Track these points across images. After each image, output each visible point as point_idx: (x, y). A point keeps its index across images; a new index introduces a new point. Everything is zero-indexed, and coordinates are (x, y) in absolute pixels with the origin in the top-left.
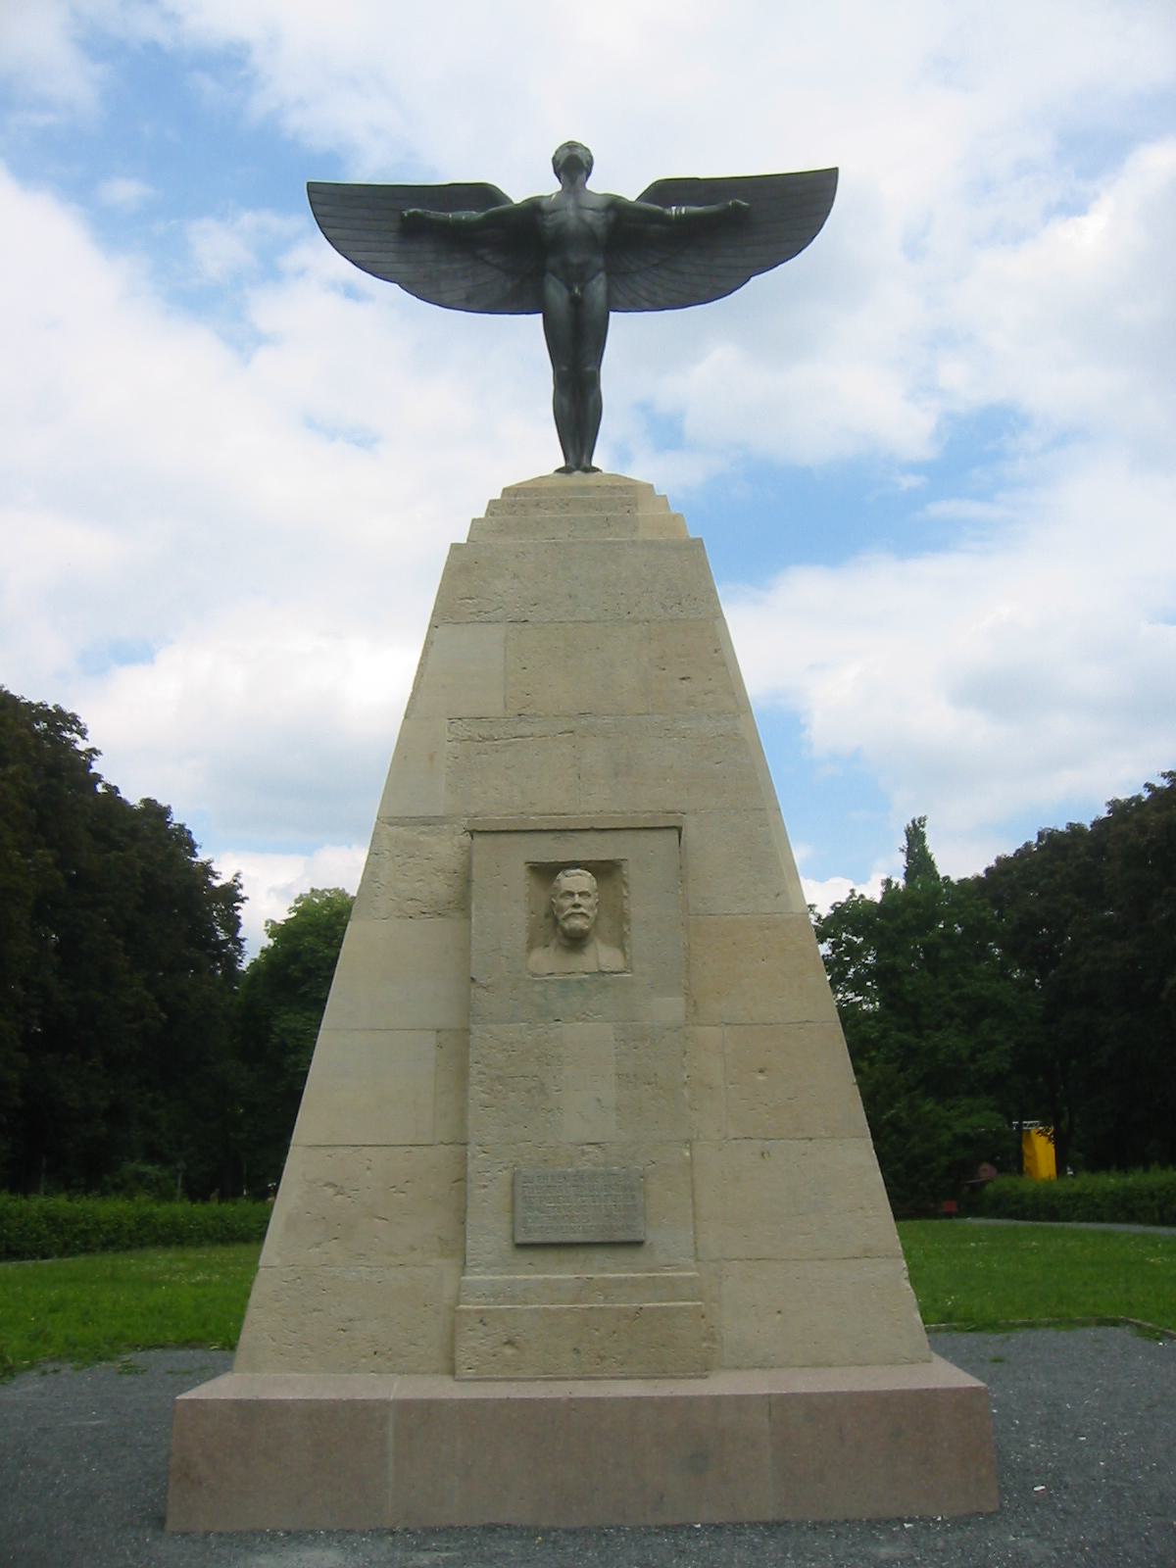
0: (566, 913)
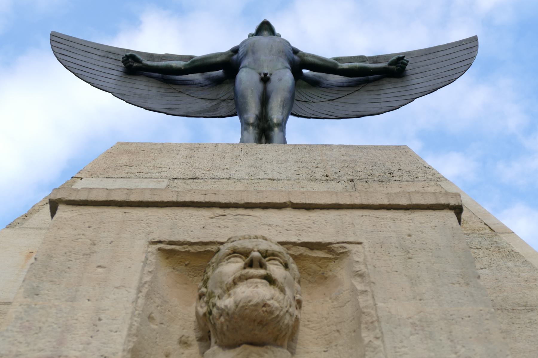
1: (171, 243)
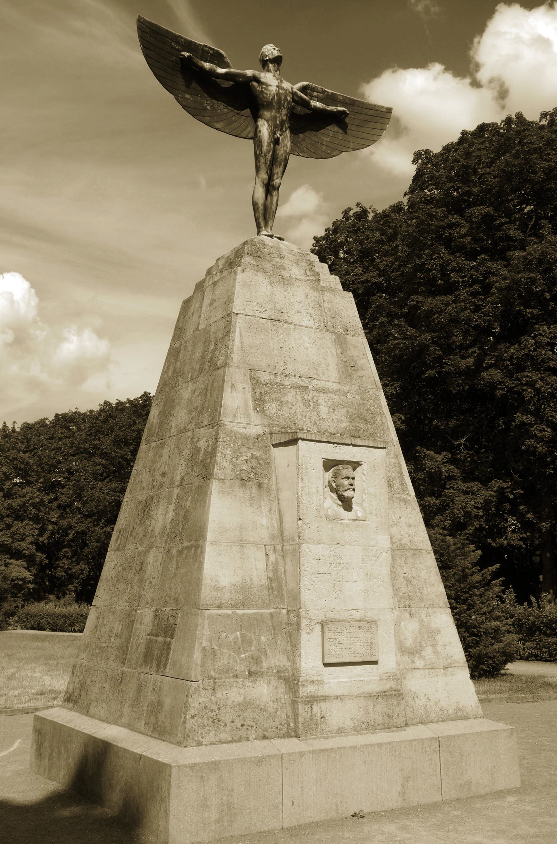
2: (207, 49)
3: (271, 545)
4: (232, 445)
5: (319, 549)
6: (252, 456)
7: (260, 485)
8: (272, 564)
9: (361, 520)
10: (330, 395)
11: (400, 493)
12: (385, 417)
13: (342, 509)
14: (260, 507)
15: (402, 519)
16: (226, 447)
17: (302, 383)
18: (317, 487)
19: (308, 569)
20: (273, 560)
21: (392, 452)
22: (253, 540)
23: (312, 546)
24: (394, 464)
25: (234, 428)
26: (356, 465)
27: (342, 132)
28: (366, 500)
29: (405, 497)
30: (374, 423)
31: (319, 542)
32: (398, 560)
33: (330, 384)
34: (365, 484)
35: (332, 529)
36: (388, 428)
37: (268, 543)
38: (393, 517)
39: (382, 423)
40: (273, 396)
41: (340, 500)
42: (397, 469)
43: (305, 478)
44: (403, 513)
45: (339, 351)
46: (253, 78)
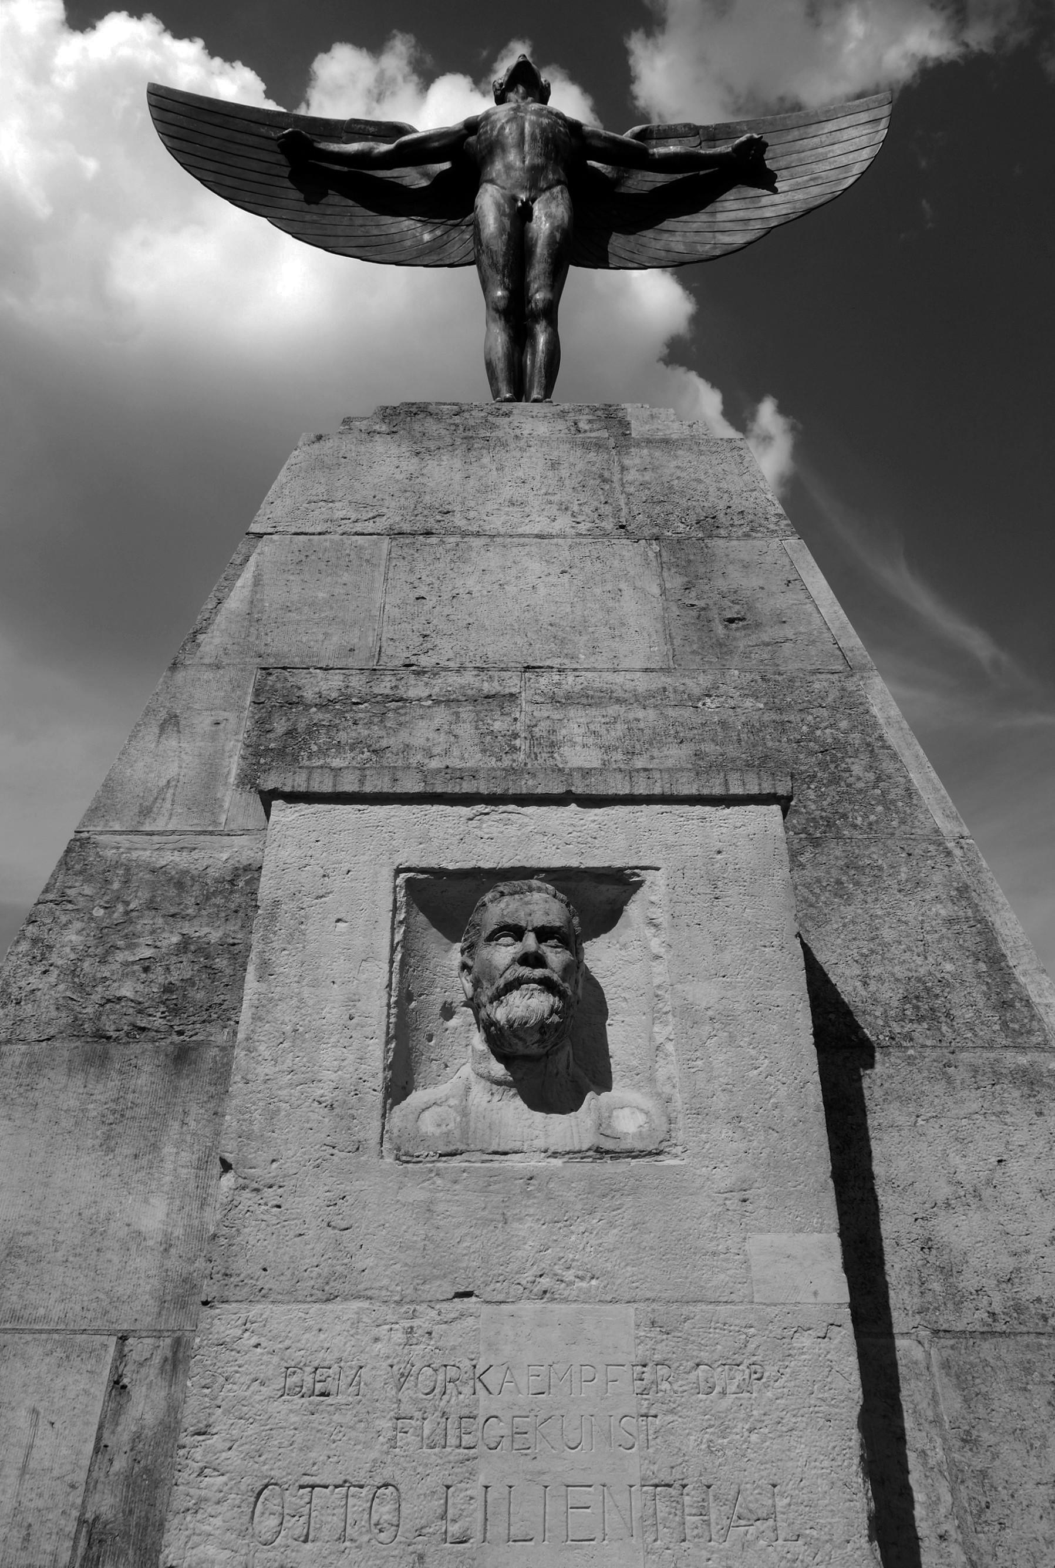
0: (501, 982)
1: (423, 871)
2: (363, 126)
3: (158, 1334)
4: (99, 912)
5: (329, 1333)
6: (185, 944)
7: (182, 1057)
8: (137, 1437)
9: (631, 1154)
10: (613, 710)
11: (990, 1046)
12: (894, 757)
13: (519, 1102)
14: (155, 1147)
15: (1013, 1166)
16: (64, 919)
17: (486, 687)
18: (353, 1000)
19: (234, 1459)
20: (150, 1419)
21: (937, 878)
22: (57, 1311)
23: (278, 1316)
24: (950, 921)
25: (134, 855)
26: (609, 891)
27: (765, 192)
28: (670, 1047)
29: (1023, 1060)
30: (835, 780)
31: (336, 1286)
32: (1005, 1399)
33: (619, 678)
34: (658, 968)
35: (429, 1208)
36: (910, 793)
37: (147, 1321)
38: (955, 1160)
39: (879, 779)
40: (342, 736)
41: (501, 1058)
42: (971, 941)
43: (286, 964)
44: (1019, 1138)
45: (675, 583)
46: (464, 132)
